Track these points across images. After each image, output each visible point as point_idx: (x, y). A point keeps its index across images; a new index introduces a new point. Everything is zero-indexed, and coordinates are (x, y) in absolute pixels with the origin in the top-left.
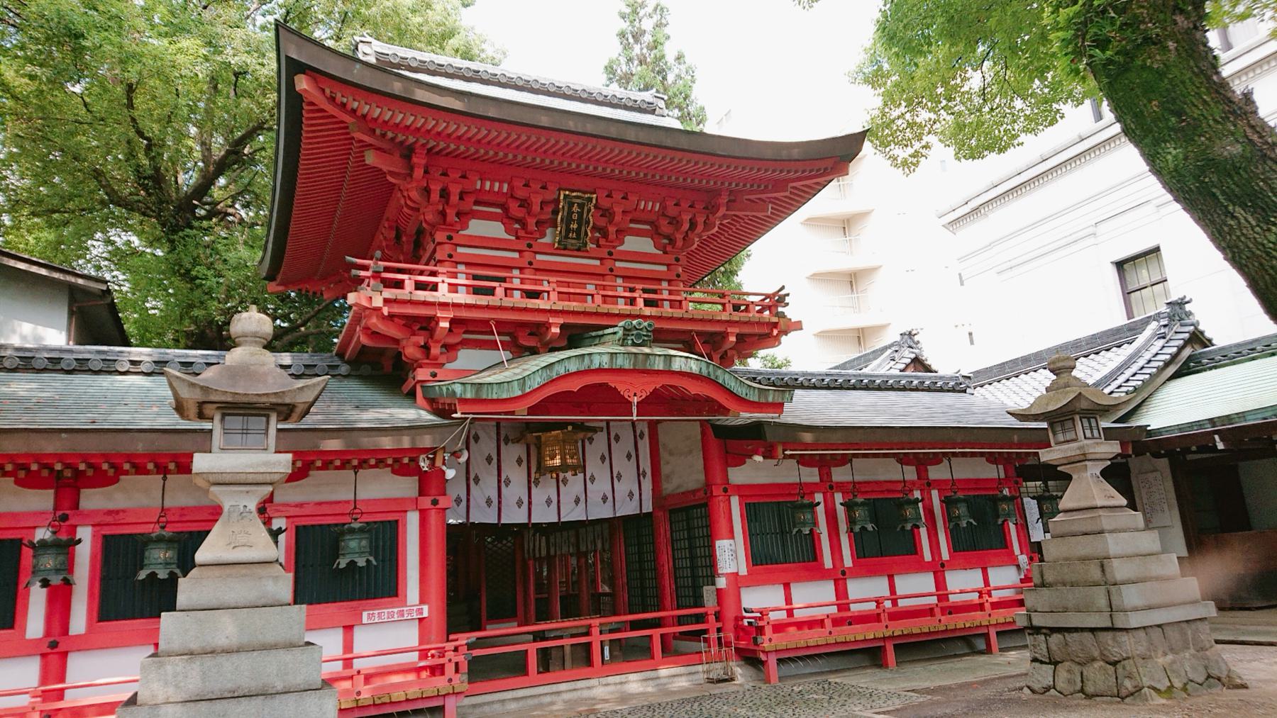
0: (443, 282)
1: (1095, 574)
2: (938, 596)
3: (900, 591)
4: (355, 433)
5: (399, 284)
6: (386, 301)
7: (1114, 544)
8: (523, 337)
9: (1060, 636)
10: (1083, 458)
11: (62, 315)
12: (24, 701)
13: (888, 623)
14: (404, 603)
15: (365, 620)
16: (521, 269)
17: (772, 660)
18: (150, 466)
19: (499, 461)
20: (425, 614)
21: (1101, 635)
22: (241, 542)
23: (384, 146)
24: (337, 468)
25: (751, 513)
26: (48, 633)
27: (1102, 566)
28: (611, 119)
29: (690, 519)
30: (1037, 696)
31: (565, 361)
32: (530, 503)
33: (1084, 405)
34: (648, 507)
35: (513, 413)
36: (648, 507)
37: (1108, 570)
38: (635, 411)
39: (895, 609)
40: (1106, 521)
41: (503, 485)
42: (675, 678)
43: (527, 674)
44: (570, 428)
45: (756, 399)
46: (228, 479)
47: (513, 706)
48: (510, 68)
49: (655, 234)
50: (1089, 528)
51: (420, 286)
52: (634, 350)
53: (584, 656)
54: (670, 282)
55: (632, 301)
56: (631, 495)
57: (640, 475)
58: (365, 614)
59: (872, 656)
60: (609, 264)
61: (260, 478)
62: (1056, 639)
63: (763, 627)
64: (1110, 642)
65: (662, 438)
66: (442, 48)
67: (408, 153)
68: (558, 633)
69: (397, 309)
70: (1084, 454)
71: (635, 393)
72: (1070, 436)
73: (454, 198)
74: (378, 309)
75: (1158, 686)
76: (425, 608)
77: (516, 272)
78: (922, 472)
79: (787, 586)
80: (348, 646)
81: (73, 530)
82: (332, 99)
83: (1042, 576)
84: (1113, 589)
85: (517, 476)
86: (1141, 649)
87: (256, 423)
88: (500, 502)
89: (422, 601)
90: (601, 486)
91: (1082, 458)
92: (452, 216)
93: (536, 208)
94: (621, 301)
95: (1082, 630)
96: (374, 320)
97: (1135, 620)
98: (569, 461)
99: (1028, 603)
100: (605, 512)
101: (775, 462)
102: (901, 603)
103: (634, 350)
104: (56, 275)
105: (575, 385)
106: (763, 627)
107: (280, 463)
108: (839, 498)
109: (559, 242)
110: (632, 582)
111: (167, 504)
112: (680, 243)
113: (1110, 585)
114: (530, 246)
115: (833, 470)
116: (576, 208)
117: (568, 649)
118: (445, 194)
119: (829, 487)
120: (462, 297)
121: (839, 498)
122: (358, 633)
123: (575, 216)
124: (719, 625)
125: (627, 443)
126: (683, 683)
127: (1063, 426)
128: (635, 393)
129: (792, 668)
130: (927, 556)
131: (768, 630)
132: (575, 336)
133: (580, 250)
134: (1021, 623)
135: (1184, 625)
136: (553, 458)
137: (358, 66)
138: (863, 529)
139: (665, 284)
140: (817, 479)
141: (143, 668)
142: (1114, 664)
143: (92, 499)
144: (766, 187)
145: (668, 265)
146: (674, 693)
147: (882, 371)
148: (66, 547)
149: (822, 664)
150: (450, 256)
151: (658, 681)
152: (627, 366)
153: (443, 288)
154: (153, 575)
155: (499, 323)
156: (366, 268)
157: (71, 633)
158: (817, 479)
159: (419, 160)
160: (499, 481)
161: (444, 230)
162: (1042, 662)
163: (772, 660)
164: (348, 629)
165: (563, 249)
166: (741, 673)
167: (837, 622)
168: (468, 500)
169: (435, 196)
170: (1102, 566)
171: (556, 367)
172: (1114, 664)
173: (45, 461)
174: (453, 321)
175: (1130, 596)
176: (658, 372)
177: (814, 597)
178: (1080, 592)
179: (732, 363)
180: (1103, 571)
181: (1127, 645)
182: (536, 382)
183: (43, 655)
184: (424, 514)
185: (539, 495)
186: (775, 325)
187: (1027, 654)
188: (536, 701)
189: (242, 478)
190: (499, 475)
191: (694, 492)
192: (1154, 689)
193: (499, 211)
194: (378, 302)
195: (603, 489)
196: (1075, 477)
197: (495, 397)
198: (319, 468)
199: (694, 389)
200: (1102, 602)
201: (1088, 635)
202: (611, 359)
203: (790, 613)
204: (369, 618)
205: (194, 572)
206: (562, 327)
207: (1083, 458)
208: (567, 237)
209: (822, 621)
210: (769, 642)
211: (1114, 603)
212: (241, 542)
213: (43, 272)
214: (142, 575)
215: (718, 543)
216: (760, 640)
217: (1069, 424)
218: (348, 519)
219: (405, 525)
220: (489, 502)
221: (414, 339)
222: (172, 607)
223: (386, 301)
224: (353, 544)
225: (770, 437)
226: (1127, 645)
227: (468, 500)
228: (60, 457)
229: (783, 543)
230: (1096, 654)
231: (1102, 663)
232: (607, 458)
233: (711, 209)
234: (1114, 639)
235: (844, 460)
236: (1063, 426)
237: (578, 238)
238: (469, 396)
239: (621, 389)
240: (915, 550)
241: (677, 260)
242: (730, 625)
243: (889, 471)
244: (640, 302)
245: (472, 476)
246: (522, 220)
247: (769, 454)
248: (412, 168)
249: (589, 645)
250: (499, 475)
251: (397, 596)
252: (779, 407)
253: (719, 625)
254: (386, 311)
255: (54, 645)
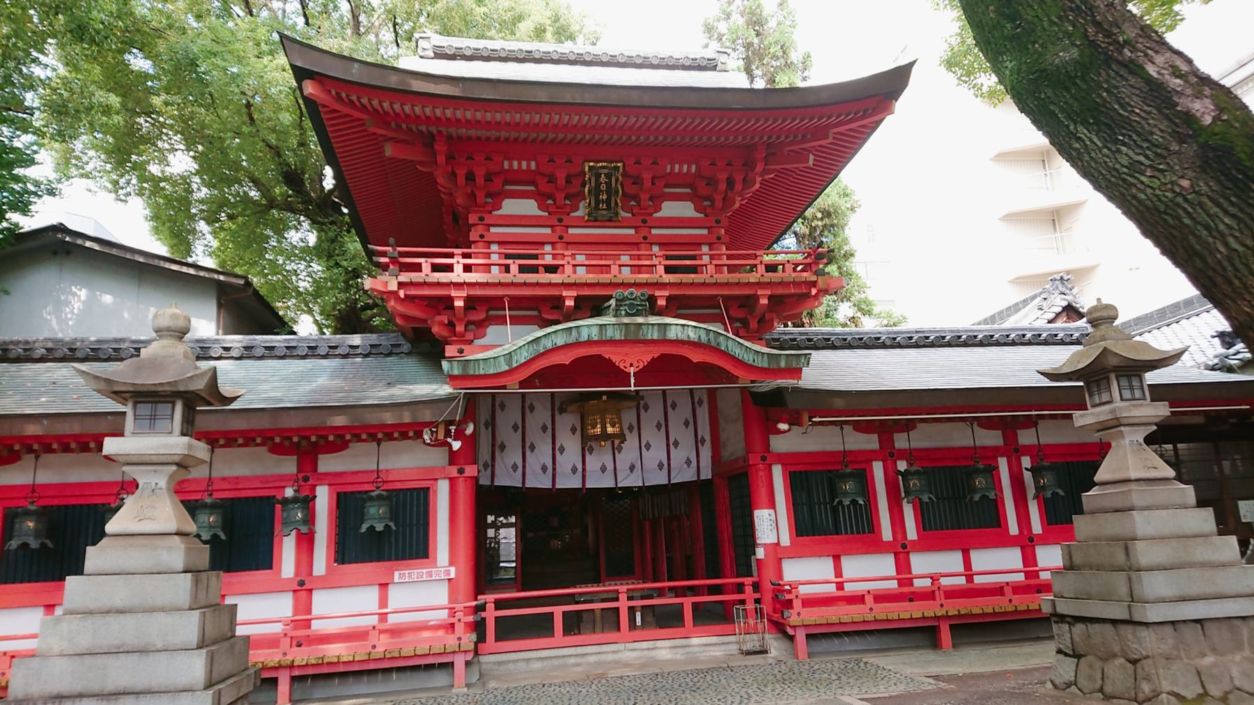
0: (458, 263)
1: (1120, 558)
2: (1026, 573)
3: (976, 567)
4: (358, 410)
5: (417, 268)
6: (401, 285)
7: (1143, 523)
8: (541, 308)
9: (1083, 626)
10: (1115, 424)
11: (211, 308)
12: (277, 628)
13: (943, 601)
14: (434, 564)
15: (396, 580)
16: (553, 244)
17: (801, 636)
18: (396, 435)
19: (667, 426)
20: (453, 576)
21: (1122, 628)
22: (149, 513)
23: (401, 137)
24: (240, 446)
25: (796, 483)
26: (297, 573)
27: (1126, 548)
28: (499, 81)
29: (732, 492)
30: (1056, 693)
31: (555, 335)
32: (584, 470)
33: (1113, 362)
34: (706, 474)
35: (504, 387)
36: (706, 474)
37: (1132, 553)
38: (632, 381)
39: (970, 586)
40: (1138, 496)
41: (557, 453)
42: (706, 646)
43: (619, 630)
44: (604, 398)
45: (765, 365)
46: (135, 460)
47: (537, 665)
48: (605, 47)
49: (695, 198)
50: (1119, 504)
51: (436, 268)
52: (626, 320)
53: (611, 620)
54: (711, 246)
55: (507, 269)
56: (688, 462)
57: (698, 442)
58: (396, 574)
59: (924, 635)
60: (644, 232)
61: (163, 459)
62: (1079, 628)
63: (790, 601)
64: (1130, 637)
65: (721, 405)
66: (513, 33)
67: (429, 141)
68: (588, 597)
69: (413, 292)
70: (1117, 419)
71: (631, 362)
72: (1105, 397)
73: (480, 181)
74: (395, 293)
75: (1183, 693)
76: (453, 569)
77: (548, 248)
78: (1010, 437)
79: (837, 559)
80: (383, 602)
81: (313, 488)
82: (339, 98)
83: (1071, 558)
84: (1134, 575)
85: (571, 445)
86: (1165, 648)
87: (164, 409)
88: (554, 469)
89: (451, 564)
90: (656, 454)
91: (1115, 423)
92: (481, 197)
93: (561, 181)
94: (495, 269)
95: (1104, 621)
96: (392, 303)
97: (1154, 614)
98: (610, 430)
99: (1055, 588)
100: (660, 479)
101: (803, 429)
102: (978, 580)
103: (626, 320)
104: (202, 274)
105: (565, 359)
106: (790, 601)
107: (178, 445)
108: (1026, 462)
109: (589, 215)
110: (677, 550)
111: (215, 474)
112: (719, 204)
113: (1132, 569)
114: (644, 221)
115: (1020, 432)
116: (603, 179)
117: (598, 613)
118: (470, 177)
119: (1013, 451)
120: (582, 274)
121: (1026, 462)
122: (392, 591)
123: (603, 187)
124: (757, 596)
125: (684, 411)
126: (717, 652)
127: (1098, 386)
128: (631, 362)
129: (824, 645)
130: (1014, 529)
131: (797, 604)
132: (592, 305)
133: (612, 221)
134: (1046, 609)
135: (1238, 622)
136: (594, 428)
137: (356, 65)
138: (854, 502)
139: (705, 249)
140: (875, 445)
141: (43, 624)
142: (1134, 662)
143: (328, 464)
144: (804, 136)
145: (709, 228)
146: (703, 662)
147: (1024, 323)
148: (308, 502)
149: (858, 644)
150: (645, 238)
151: (688, 650)
152: (618, 337)
153: (458, 268)
154: (25, 546)
155: (727, 299)
156: (384, 254)
157: (315, 574)
158: (875, 445)
159: (440, 147)
160: (554, 449)
161: (476, 212)
162: (1066, 655)
163: (801, 636)
164: (384, 586)
165: (594, 221)
166: (776, 647)
167: (1017, 589)
168: (524, 467)
169: (461, 180)
170: (1126, 548)
171: (543, 341)
172: (1134, 662)
173: (286, 433)
174: (577, 299)
175: (1155, 585)
176: (653, 341)
177: (869, 571)
178: (1105, 576)
179: (772, 327)
180: (1127, 554)
181: (1148, 642)
182: (523, 357)
183: (295, 591)
184: (452, 481)
185: (593, 462)
186: (814, 284)
187: (1051, 647)
188: (561, 661)
189: (147, 459)
190: (554, 443)
191: (737, 460)
192: (1177, 696)
193: (688, 190)
194: (393, 286)
195: (653, 456)
196: (1113, 444)
197: (482, 372)
198: (222, 446)
199: (696, 357)
200: (1123, 590)
201: (1108, 627)
202: (601, 331)
203: (840, 586)
204: (400, 577)
205: (104, 541)
206: (770, 297)
207: (1115, 424)
208: (597, 208)
209: (1002, 588)
210: (795, 616)
211: (1135, 592)
212: (149, 513)
213: (192, 271)
214: (14, 544)
215: (757, 513)
216: (786, 614)
217: (1103, 384)
218: (22, 503)
219: (435, 492)
220: (544, 469)
221: (438, 318)
222: (78, 570)
223: (401, 285)
224: (373, 510)
225: (792, 403)
226: (1148, 642)
227: (524, 467)
228: (297, 431)
229: (830, 512)
230: (1117, 649)
231: (1122, 660)
232: (521, 428)
233: (749, 165)
234: (1134, 634)
235: (1030, 423)
236: (1098, 386)
237: (609, 208)
238: (456, 372)
239: (616, 359)
240: (998, 520)
241: (718, 222)
242: (768, 597)
243: (960, 437)
244: (661, 269)
245: (528, 444)
246: (557, 196)
247: (795, 421)
248: (434, 155)
249: (618, 609)
250: (554, 443)
251: (427, 557)
252: (797, 373)
253: (757, 596)
254: (402, 294)
255: (302, 583)
